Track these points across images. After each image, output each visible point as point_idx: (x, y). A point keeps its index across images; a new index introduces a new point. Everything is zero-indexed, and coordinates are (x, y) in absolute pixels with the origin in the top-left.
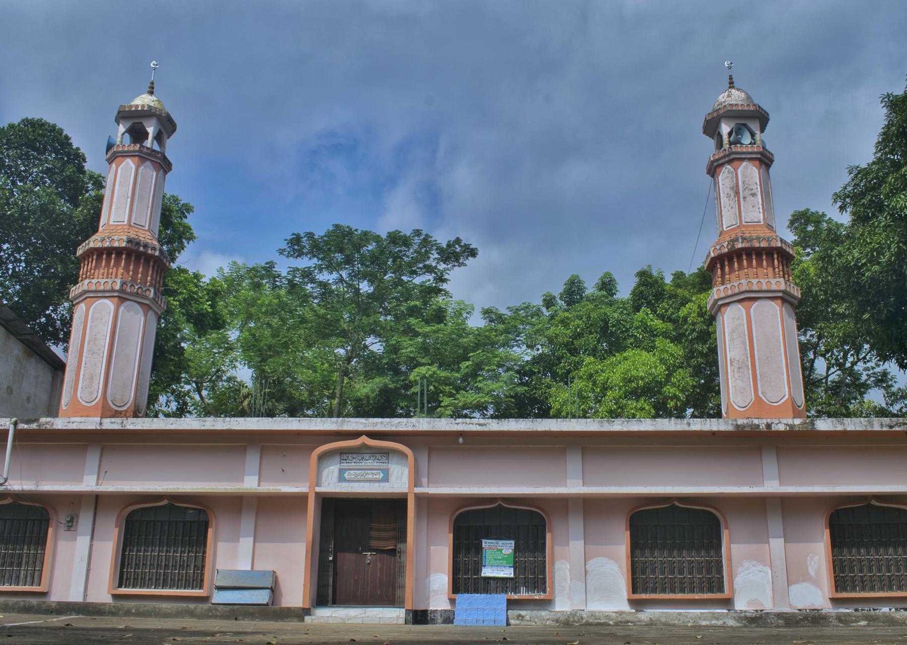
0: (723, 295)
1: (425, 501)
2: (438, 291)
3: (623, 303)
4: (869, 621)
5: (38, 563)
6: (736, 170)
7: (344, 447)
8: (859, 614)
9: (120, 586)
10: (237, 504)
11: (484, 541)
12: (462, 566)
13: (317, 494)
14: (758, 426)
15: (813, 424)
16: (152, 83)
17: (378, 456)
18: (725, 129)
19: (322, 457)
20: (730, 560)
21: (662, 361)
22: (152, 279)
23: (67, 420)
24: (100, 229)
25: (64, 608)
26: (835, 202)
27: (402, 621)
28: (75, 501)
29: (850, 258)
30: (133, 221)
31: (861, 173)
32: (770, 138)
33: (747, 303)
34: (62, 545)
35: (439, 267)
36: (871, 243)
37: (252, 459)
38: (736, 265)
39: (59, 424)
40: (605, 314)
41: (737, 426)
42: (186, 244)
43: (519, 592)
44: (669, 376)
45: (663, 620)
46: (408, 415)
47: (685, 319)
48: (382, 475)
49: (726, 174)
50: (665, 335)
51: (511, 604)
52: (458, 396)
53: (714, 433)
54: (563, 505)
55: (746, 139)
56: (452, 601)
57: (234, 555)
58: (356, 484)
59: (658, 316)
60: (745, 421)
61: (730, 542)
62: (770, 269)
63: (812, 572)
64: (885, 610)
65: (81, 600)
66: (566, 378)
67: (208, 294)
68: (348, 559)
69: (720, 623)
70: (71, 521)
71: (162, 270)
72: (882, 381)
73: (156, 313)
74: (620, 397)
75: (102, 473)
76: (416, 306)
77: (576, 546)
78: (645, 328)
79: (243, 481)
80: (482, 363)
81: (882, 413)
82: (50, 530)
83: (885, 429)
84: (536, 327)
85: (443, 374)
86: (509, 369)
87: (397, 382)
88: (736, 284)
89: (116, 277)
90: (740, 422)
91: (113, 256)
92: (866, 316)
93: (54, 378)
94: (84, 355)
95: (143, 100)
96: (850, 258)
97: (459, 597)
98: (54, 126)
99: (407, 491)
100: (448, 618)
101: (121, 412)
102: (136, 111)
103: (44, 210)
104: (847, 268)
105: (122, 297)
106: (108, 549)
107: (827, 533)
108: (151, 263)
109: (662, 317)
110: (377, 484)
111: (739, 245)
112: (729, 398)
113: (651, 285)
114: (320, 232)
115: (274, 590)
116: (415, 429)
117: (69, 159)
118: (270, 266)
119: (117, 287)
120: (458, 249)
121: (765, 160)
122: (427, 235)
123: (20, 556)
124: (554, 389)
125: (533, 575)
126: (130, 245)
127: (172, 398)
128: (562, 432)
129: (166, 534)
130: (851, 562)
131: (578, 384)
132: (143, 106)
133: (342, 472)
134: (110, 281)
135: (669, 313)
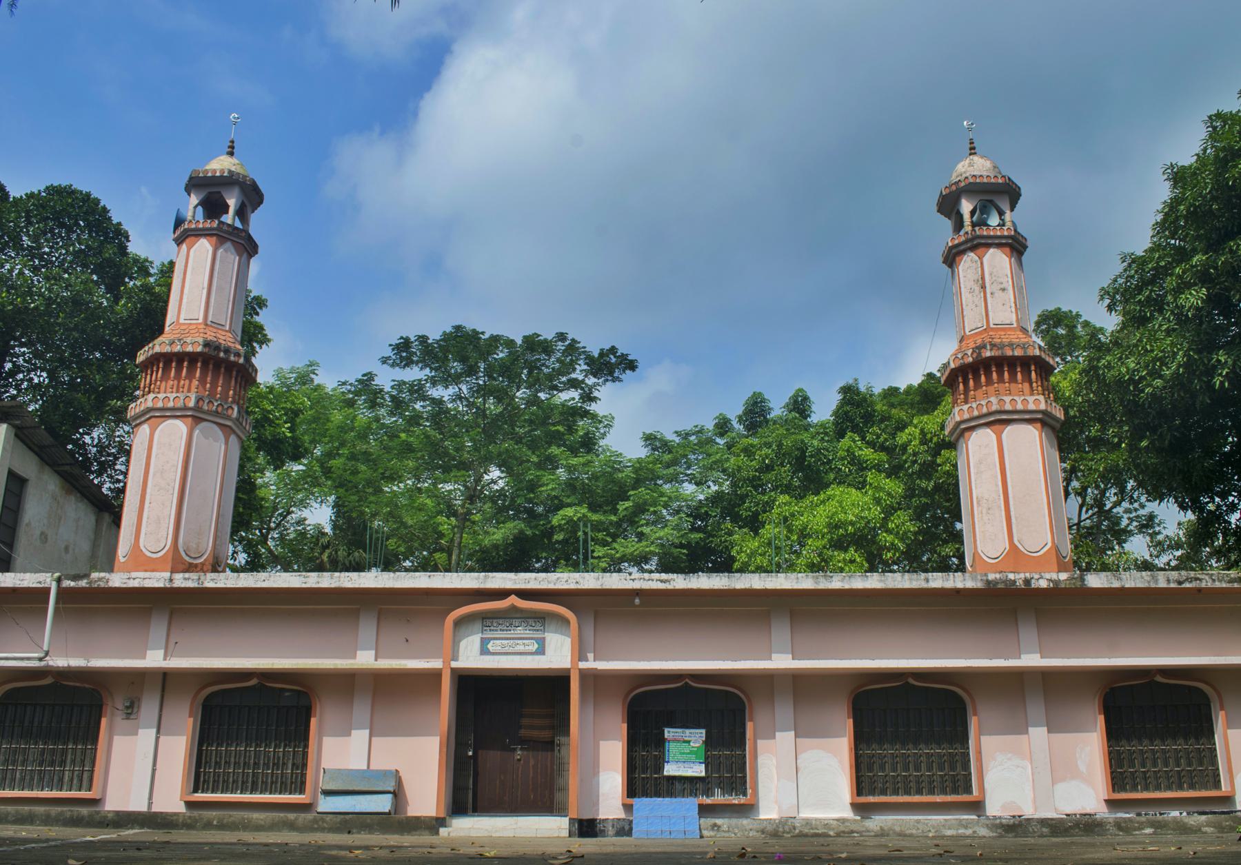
0: (966, 416)
1: (592, 680)
2: (586, 414)
3: (823, 425)
4: (1156, 828)
5: (87, 762)
6: (981, 258)
7: (492, 613)
8: (1143, 819)
9: (195, 790)
10: (347, 684)
11: (666, 730)
12: (638, 763)
13: (453, 670)
14: (1014, 581)
15: (1083, 580)
16: (232, 142)
17: (531, 622)
18: (966, 207)
19: (459, 623)
20: (979, 752)
21: (878, 501)
22: (235, 394)
23: (126, 575)
24: (167, 329)
25: (125, 819)
26: (1102, 299)
27: (565, 833)
28: (137, 680)
29: (1124, 370)
30: (210, 319)
31: (1136, 262)
32: (1019, 218)
33: (997, 427)
34: (118, 741)
35: (587, 381)
36: (1152, 351)
37: (367, 628)
38: (983, 378)
39: (117, 580)
40: (802, 441)
41: (988, 582)
42: (258, 349)
43: (713, 795)
44: (885, 520)
45: (897, 829)
46: (545, 570)
47: (904, 448)
48: (536, 646)
49: (969, 263)
50: (878, 468)
51: (704, 810)
52: (615, 545)
53: (957, 592)
54: (768, 682)
55: (994, 220)
56: (628, 808)
57: (344, 751)
58: (503, 658)
59: (867, 443)
60: (998, 576)
61: (980, 733)
62: (1026, 385)
63: (1082, 768)
64: (1175, 814)
65: (144, 809)
66: (754, 524)
67: (286, 414)
68: (492, 758)
69: (969, 832)
70: (131, 706)
71: (247, 381)
72: (1146, 526)
73: (238, 437)
74: (824, 547)
75: (171, 645)
76: (558, 431)
77: (785, 738)
78: (852, 460)
79: (354, 657)
80: (645, 503)
81: (1146, 566)
82: (104, 721)
83: (1172, 585)
84: (713, 459)
85: (595, 517)
86: (677, 512)
87: (536, 527)
88: (983, 403)
89: (189, 391)
90: (991, 577)
91: (186, 364)
92: (1144, 444)
93: (97, 521)
94: (148, 491)
95: (221, 164)
96: (1124, 370)
97: (636, 802)
98: (88, 195)
99: (568, 665)
100: (624, 829)
101: (196, 566)
102: (214, 177)
103: (77, 303)
104: (1119, 382)
105: (196, 416)
106: (177, 749)
107: (1101, 719)
108: (234, 373)
109: (871, 444)
110: (530, 657)
111: (988, 354)
112: (976, 547)
113: (858, 405)
114: (434, 335)
115: (398, 794)
116: (579, 587)
117: (106, 238)
118: (370, 376)
119: (192, 404)
120: (614, 360)
121: (1016, 246)
122: (573, 340)
123: (64, 752)
124: (736, 537)
125: (729, 771)
126: (206, 350)
127: (240, 548)
128: (692, 590)
129: (253, 724)
130: (1188, 754)
131: (769, 531)
132: (222, 171)
133: (484, 642)
134: (182, 396)
135: (882, 439)
